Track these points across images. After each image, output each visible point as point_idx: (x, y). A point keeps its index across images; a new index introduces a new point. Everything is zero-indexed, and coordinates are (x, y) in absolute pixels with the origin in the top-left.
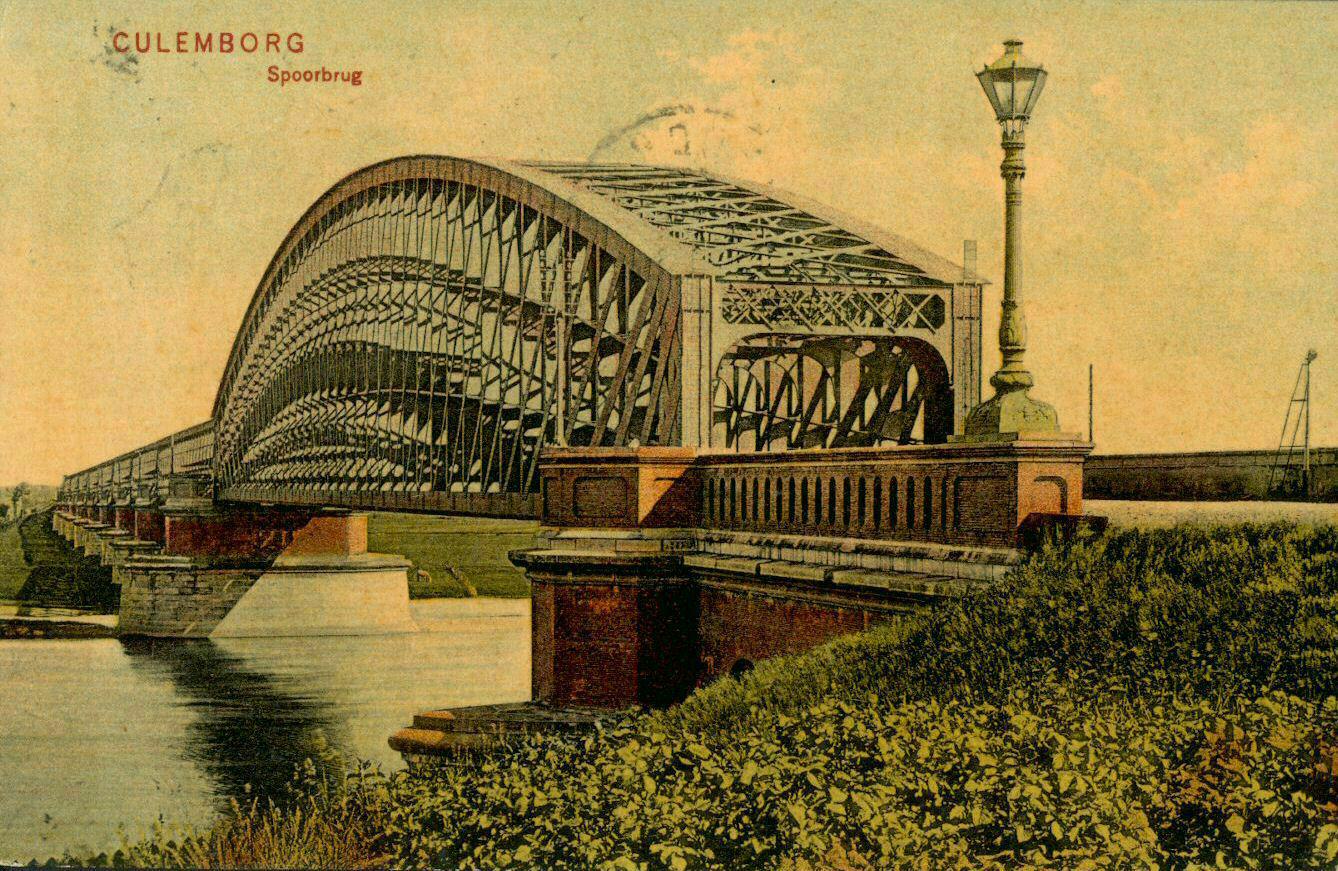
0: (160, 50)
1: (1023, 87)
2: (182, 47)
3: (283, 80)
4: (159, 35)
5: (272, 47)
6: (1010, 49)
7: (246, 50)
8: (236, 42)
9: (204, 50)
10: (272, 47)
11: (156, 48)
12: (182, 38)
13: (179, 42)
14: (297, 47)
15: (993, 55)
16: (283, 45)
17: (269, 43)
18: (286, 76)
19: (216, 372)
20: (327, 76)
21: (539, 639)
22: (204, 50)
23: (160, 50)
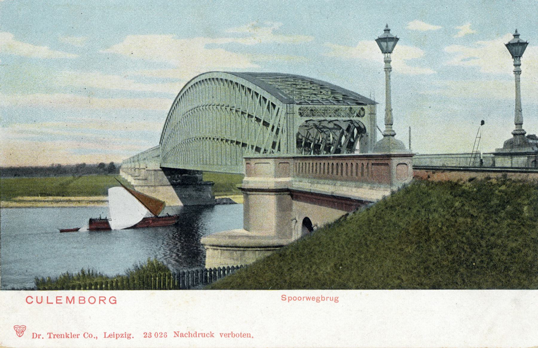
0: (48, 303)
1: (391, 44)
2: (58, 301)
3: (289, 300)
4: (48, 297)
5: (101, 302)
6: (248, 162)
7: (38, 303)
8: (87, 300)
9: (70, 303)
10: (101, 302)
11: (46, 301)
12: (58, 298)
13: (57, 300)
14: (114, 302)
15: (381, 33)
16: (107, 301)
17: (100, 300)
18: (290, 299)
19: (361, 293)
20: (323, 299)
21: (376, 284)
22: (70, 303)
23: (48, 303)
